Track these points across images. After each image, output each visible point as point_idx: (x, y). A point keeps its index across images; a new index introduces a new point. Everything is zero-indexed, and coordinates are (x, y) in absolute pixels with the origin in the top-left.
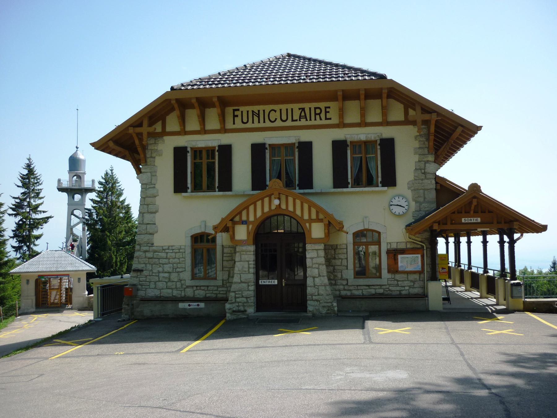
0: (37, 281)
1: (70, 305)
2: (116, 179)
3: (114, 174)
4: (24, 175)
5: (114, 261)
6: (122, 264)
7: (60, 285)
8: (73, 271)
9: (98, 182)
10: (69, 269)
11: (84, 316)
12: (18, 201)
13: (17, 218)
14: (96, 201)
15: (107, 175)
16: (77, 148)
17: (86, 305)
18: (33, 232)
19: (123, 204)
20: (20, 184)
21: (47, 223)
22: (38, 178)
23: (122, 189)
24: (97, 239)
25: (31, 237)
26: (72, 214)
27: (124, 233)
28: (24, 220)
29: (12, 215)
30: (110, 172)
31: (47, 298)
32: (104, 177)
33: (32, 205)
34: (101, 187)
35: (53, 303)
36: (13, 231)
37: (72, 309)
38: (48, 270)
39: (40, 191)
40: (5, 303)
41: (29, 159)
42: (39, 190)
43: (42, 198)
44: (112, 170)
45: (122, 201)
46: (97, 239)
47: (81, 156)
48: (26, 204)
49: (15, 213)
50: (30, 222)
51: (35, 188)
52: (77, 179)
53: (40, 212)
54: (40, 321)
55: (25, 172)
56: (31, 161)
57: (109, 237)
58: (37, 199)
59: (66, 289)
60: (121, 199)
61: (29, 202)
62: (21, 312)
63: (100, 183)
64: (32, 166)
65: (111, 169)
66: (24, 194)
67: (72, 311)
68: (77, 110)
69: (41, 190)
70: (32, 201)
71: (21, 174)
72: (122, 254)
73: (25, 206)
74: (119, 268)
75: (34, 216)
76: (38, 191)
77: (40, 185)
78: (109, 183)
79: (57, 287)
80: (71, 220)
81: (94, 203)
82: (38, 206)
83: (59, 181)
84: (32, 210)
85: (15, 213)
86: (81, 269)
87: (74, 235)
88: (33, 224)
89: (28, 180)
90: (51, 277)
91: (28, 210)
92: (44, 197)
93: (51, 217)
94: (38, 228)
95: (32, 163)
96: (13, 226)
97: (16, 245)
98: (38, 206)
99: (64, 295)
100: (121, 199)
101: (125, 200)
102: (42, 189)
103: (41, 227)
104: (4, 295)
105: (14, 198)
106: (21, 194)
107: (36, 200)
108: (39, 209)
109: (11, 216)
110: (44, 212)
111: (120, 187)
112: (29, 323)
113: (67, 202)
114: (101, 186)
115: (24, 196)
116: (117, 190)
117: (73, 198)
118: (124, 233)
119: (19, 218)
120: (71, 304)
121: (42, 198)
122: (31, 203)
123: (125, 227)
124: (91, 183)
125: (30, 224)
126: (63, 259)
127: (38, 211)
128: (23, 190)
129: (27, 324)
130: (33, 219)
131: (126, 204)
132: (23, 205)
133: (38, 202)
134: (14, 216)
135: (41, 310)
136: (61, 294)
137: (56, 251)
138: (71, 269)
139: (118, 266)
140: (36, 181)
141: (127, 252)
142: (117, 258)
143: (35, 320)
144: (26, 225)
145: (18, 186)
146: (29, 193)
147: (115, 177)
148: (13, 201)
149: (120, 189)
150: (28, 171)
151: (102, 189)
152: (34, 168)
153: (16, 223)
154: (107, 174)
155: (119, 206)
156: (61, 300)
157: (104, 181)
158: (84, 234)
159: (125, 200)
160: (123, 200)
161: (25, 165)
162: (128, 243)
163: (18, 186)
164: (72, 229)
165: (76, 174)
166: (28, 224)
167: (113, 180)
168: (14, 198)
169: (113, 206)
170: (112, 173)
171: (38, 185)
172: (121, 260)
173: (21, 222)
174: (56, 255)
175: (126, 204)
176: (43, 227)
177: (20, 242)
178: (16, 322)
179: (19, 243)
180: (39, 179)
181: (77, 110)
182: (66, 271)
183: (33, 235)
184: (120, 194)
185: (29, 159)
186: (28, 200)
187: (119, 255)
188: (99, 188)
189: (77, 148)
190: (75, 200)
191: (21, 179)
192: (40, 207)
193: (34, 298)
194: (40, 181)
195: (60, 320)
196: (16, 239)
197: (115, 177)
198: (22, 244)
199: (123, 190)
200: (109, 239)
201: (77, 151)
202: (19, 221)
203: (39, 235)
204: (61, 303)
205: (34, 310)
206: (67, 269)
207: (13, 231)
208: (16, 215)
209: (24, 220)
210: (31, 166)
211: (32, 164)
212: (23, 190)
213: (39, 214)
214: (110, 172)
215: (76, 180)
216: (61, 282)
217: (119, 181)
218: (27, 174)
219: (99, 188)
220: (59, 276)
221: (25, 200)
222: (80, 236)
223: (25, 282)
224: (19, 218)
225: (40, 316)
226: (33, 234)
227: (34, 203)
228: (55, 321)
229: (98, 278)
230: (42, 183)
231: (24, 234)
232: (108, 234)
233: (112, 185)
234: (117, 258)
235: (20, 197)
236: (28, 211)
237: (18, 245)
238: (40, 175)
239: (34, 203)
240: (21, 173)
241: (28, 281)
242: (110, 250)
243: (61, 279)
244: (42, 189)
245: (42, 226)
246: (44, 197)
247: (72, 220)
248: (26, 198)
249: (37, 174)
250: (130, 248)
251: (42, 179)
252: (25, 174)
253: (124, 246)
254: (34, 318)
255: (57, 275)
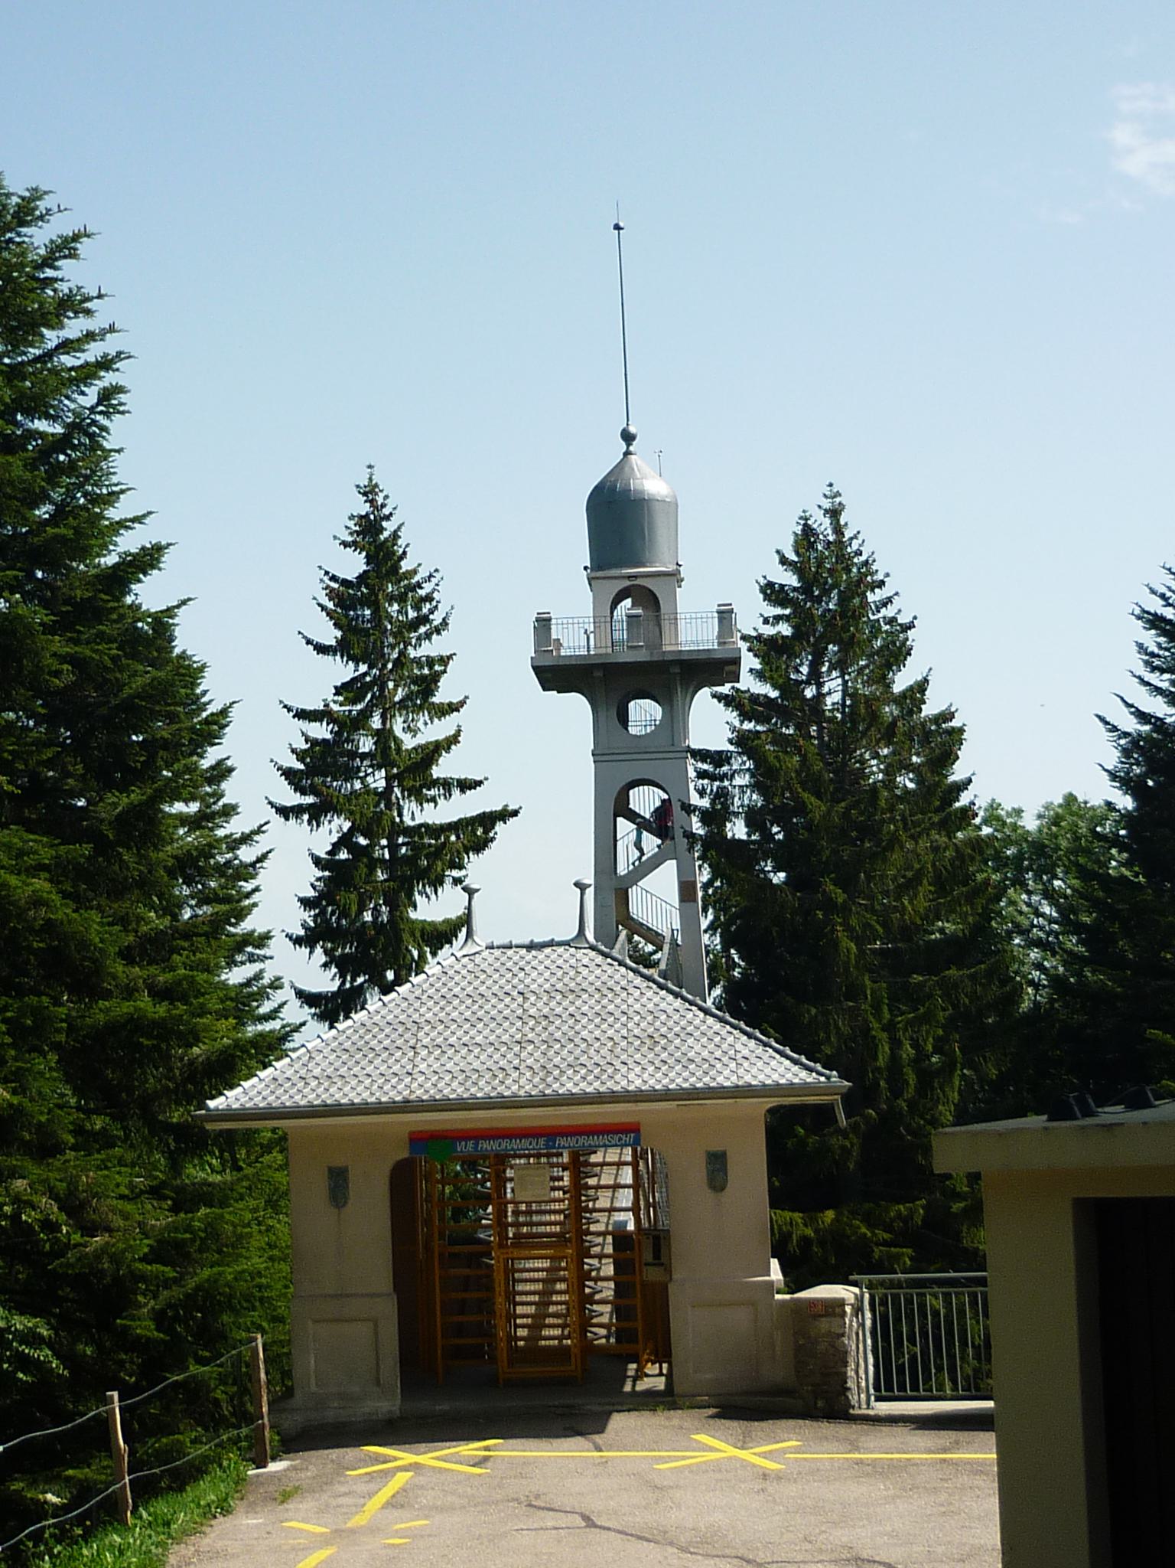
0: (402, 1178)
1: (652, 1369)
2: (866, 563)
3: (848, 534)
4: (345, 583)
5: (882, 1061)
6: (927, 1079)
7: (578, 1212)
8: (666, 1095)
9: (763, 590)
10: (635, 1080)
11: (779, 1477)
12: (321, 731)
13: (325, 827)
14: (755, 699)
15: (811, 546)
16: (628, 437)
17: (778, 1372)
18: (415, 907)
19: (911, 712)
20: (330, 635)
21: (487, 851)
22: (422, 592)
23: (903, 619)
24: (775, 930)
25: (406, 936)
26: (622, 809)
27: (926, 888)
28: (363, 841)
29: (297, 811)
30: (823, 525)
31: (486, 1307)
32: (792, 556)
33: (399, 749)
34: (778, 619)
35: (534, 1353)
36: (306, 903)
37: (666, 1400)
38: (481, 1090)
39: (437, 668)
40: (222, 1336)
41: (369, 492)
42: (431, 662)
43: (453, 708)
44: (834, 513)
45: (904, 695)
46: (775, 930)
47: (651, 484)
48: (366, 744)
49: (310, 800)
50: (393, 847)
51: (412, 653)
52: (640, 611)
53: (446, 785)
54: (427, 1511)
55: (353, 565)
56: (380, 500)
57: (845, 910)
58: (423, 718)
59: (621, 1239)
60: (901, 682)
61: (384, 736)
62: (292, 1422)
63: (772, 593)
64: (389, 526)
65: (827, 504)
66: (349, 690)
67: (677, 1417)
68: (617, 227)
69: (444, 660)
70: (398, 726)
71: (334, 578)
72: (927, 1018)
73: (363, 756)
74: (911, 1104)
75: (415, 814)
76: (426, 671)
77: (438, 631)
78: (826, 592)
79: (551, 1223)
80: (615, 841)
81: (745, 716)
82: (433, 752)
83: (543, 624)
84: (399, 777)
85: (310, 800)
86: (726, 1078)
87: (636, 928)
88: (411, 861)
89: (368, 612)
90: (506, 1145)
91: (378, 780)
92: (462, 703)
93: (505, 815)
94: (437, 882)
95: (386, 511)
96: (306, 879)
97: (327, 982)
98: (433, 752)
99: (608, 1290)
100: (901, 682)
101: (921, 686)
102: (450, 657)
103: (456, 873)
104: (213, 1281)
105: (302, 715)
106: (338, 691)
107: (420, 724)
108: (437, 772)
109: (292, 821)
110: (466, 785)
111: (889, 612)
112: (339, 1534)
113: (592, 747)
114: (779, 611)
115: (354, 702)
116: (876, 628)
117: (623, 719)
118: (926, 888)
119: (336, 825)
120: (663, 1354)
121: (453, 708)
122: (395, 739)
123: (935, 849)
124: (714, 627)
125: (390, 865)
126: (587, 1004)
127: (435, 783)
128: (343, 671)
129: (325, 1541)
130: (409, 831)
131: (930, 708)
132: (354, 754)
133: (433, 731)
134: (306, 817)
135: (443, 1407)
136: (583, 1276)
137: (531, 947)
138: (655, 1081)
139: (910, 1092)
140: (412, 614)
141: (955, 1007)
142: (896, 1044)
143: (392, 1504)
144: (374, 864)
145: (321, 649)
146: (380, 680)
147: (859, 553)
148: (297, 733)
149: (892, 621)
150: (369, 560)
151: (785, 629)
152: (395, 536)
153: (317, 861)
154: (807, 536)
155: (894, 724)
156: (585, 1323)
157: (791, 580)
158: (689, 922)
159: (921, 686)
160: (911, 688)
161: (351, 524)
162: (957, 950)
163: (321, 649)
164: (623, 897)
165: (627, 583)
166: (382, 861)
167: (848, 571)
168: (302, 715)
169: (854, 728)
170: (838, 530)
171: (428, 636)
172: (921, 1056)
173: (343, 855)
174: (537, 980)
175: (930, 708)
176: (463, 873)
177: (343, 965)
178: (252, 1508)
179: (343, 976)
180: (429, 598)
181: (617, 227)
182: (613, 1097)
183: (413, 922)
184: (896, 654)
185: (369, 492)
186: (376, 722)
187: (909, 1023)
188: (766, 621)
189: (628, 437)
190: (632, 730)
191: (330, 605)
192: (444, 759)
193: (388, 1310)
194: (432, 612)
195: (594, 1505)
196: (326, 952)
197: (859, 553)
198: (360, 980)
199: (910, 626)
200: (848, 928)
201: (627, 453)
202: (336, 847)
203: (447, 921)
204: (588, 1348)
205: (387, 1404)
206: (619, 1084)
207: (306, 903)
208: (316, 814)
209: (363, 841)
210: (382, 529)
211: (388, 518)
212: (343, 671)
213: (441, 801)
214: (827, 521)
215: (628, 616)
216: (578, 1189)
217: (879, 577)
218: (362, 578)
219: (766, 621)
220: (561, 1141)
221: (359, 722)
222: (667, 934)
223: (321, 1185)
224: (336, 825)
225: (431, 1456)
226: (413, 915)
227: (409, 742)
228: (550, 1520)
229: (1036, 1121)
230: (445, 623)
231: (368, 917)
232: (840, 896)
233: (843, 600)
234: (896, 1044)
235: (335, 707)
236: (381, 784)
237: (334, 986)
238: (431, 576)
239: (409, 742)
240: (332, 572)
241: (338, 1181)
242: (854, 992)
243: (579, 1167)
244: (450, 657)
245: (461, 867)
246: (462, 703)
247: (619, 844)
248: (366, 714)
249: (415, 572)
250: (973, 977)
251: (447, 599)
252: (351, 576)
253: (930, 970)
254: (388, 1474)
255: (551, 1134)
